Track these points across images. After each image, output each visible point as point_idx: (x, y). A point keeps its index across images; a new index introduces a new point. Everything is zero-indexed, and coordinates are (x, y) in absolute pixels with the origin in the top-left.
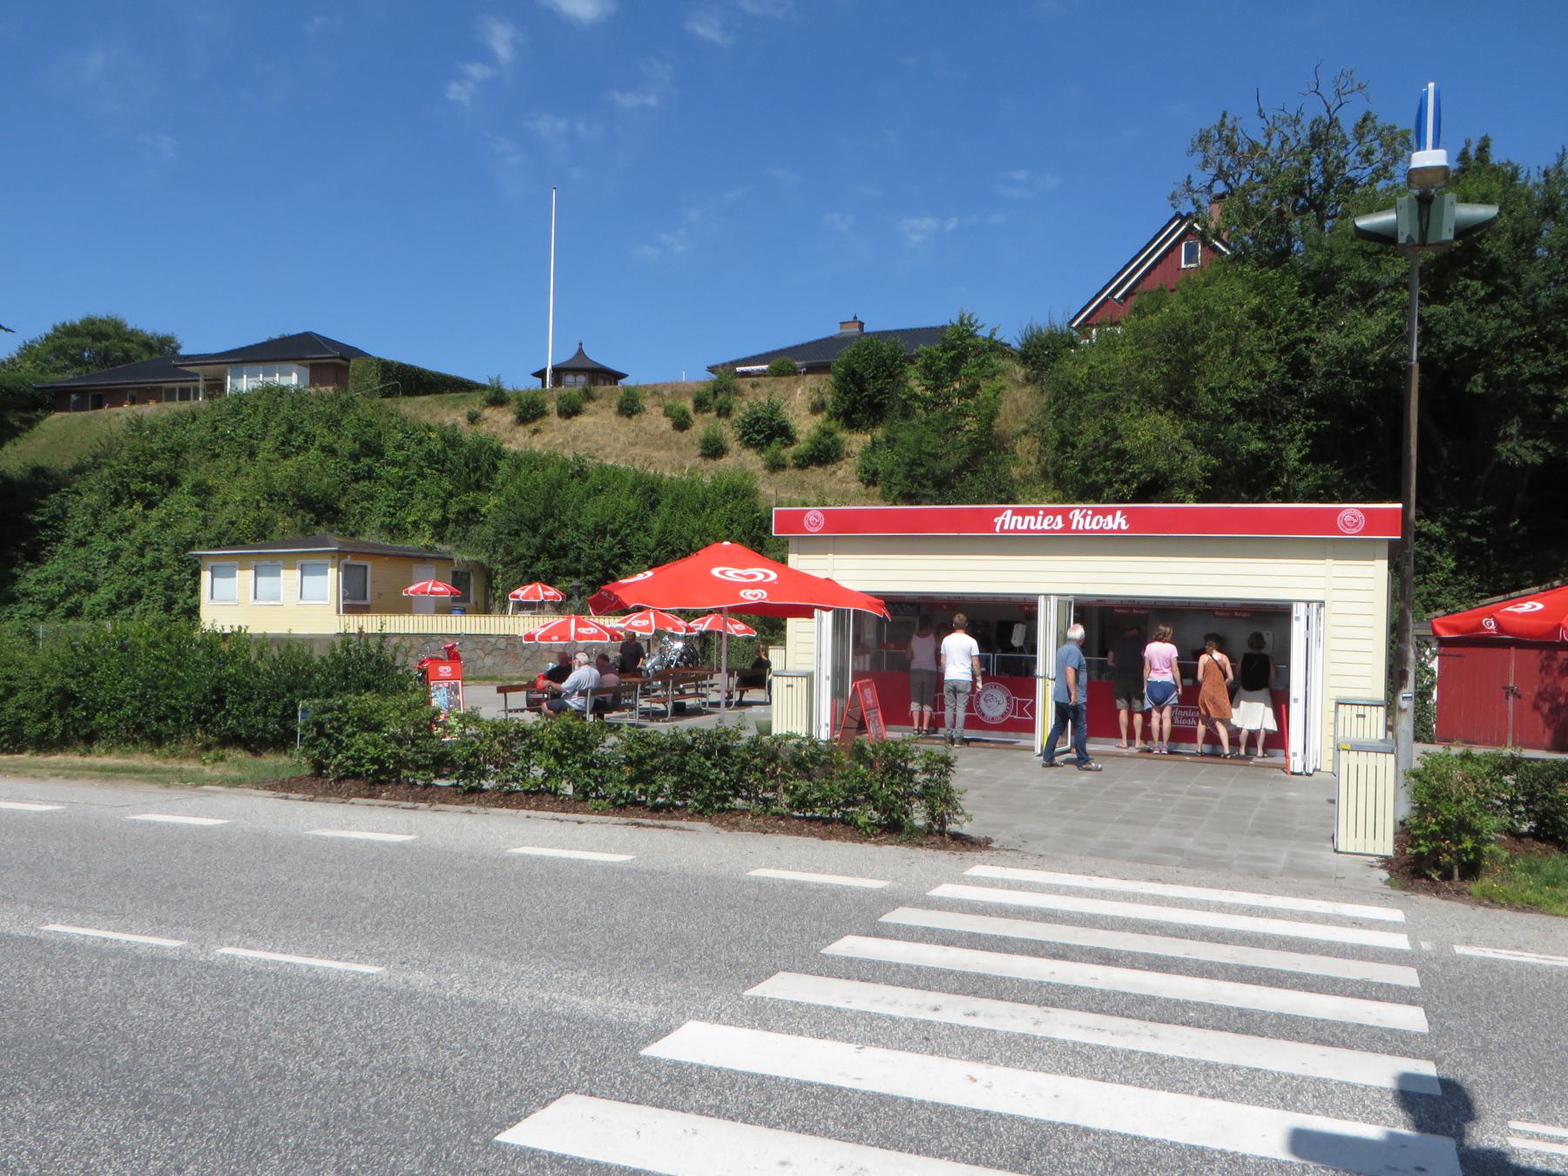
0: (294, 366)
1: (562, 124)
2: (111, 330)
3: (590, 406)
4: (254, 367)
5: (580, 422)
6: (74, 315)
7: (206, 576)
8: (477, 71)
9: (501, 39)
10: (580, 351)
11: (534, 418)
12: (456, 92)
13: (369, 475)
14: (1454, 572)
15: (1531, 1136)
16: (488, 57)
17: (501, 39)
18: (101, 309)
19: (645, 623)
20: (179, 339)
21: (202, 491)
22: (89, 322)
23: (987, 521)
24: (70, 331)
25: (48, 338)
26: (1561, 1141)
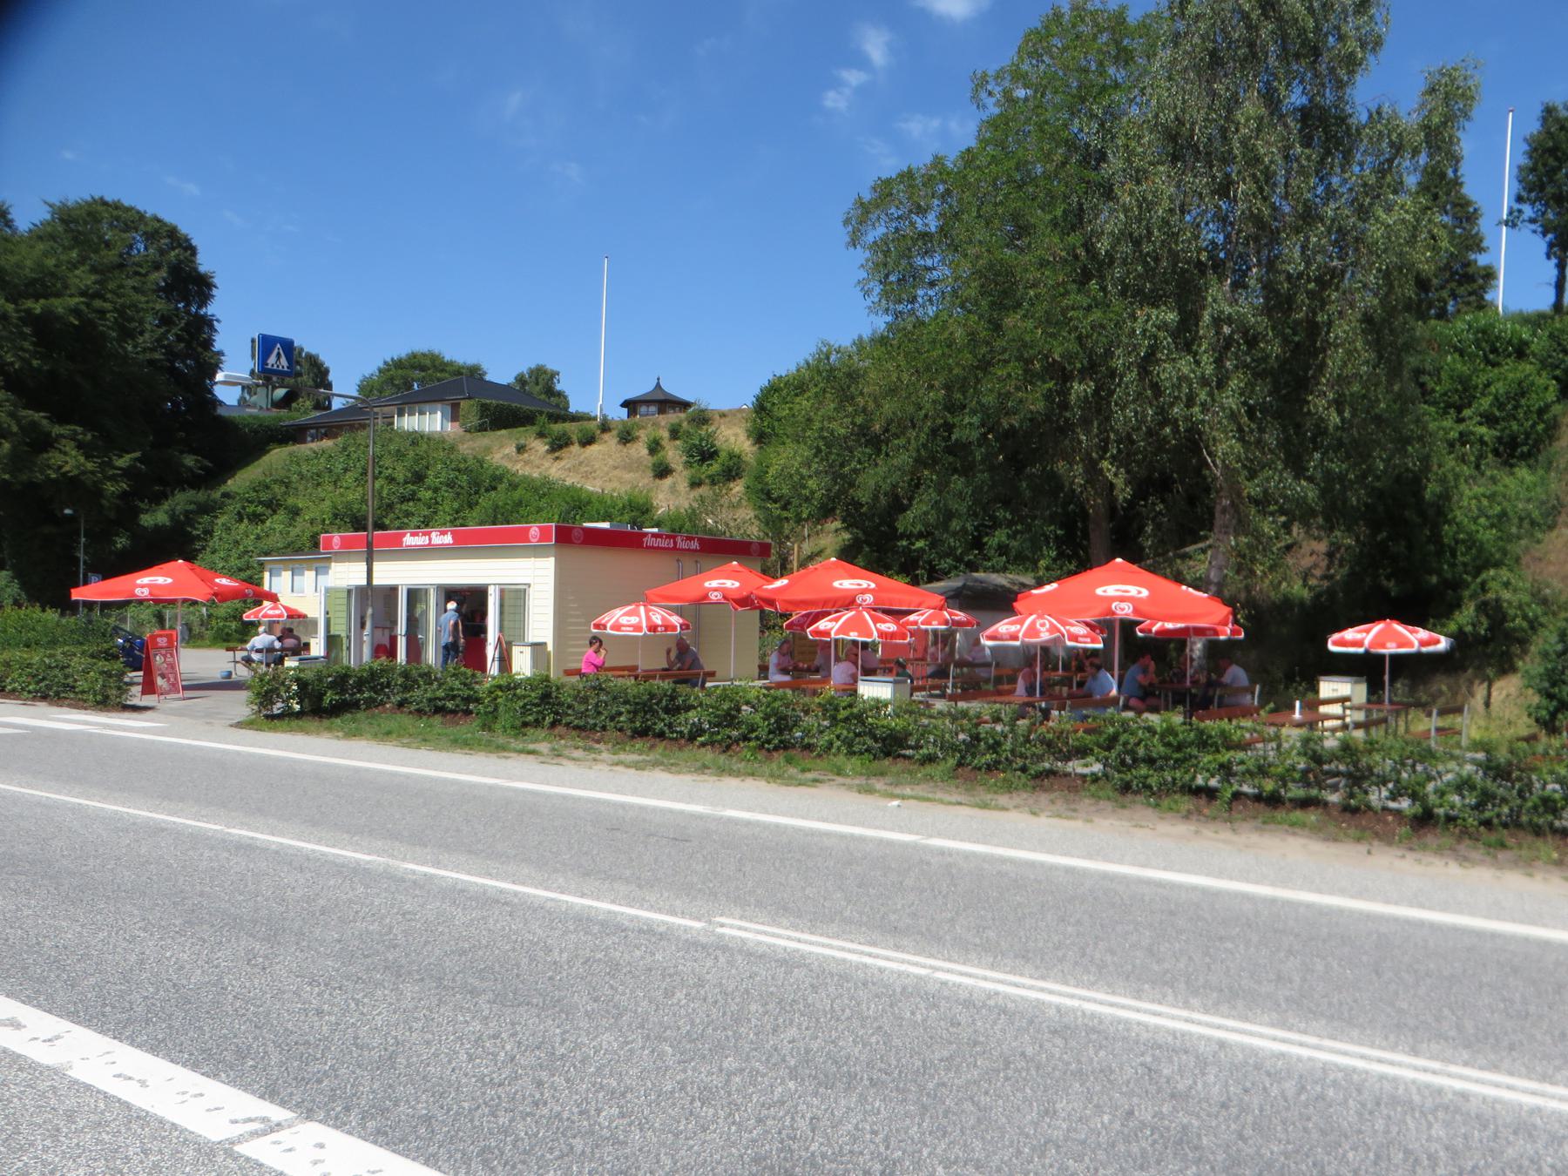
0: (439, 405)
1: (935, 123)
2: (428, 362)
3: (606, 436)
4: (433, 405)
5: (594, 448)
6: (400, 350)
7: (267, 575)
8: (854, 77)
9: (876, 45)
10: (658, 385)
11: (560, 447)
12: (833, 100)
13: (413, 497)
14: (1054, 560)
15: (1400, 1065)
16: (862, 62)
17: (876, 45)
19: (634, 620)
20: (485, 366)
21: (295, 512)
22: (414, 356)
23: (398, 540)
24: (399, 364)
25: (380, 371)
26: (1562, 1099)
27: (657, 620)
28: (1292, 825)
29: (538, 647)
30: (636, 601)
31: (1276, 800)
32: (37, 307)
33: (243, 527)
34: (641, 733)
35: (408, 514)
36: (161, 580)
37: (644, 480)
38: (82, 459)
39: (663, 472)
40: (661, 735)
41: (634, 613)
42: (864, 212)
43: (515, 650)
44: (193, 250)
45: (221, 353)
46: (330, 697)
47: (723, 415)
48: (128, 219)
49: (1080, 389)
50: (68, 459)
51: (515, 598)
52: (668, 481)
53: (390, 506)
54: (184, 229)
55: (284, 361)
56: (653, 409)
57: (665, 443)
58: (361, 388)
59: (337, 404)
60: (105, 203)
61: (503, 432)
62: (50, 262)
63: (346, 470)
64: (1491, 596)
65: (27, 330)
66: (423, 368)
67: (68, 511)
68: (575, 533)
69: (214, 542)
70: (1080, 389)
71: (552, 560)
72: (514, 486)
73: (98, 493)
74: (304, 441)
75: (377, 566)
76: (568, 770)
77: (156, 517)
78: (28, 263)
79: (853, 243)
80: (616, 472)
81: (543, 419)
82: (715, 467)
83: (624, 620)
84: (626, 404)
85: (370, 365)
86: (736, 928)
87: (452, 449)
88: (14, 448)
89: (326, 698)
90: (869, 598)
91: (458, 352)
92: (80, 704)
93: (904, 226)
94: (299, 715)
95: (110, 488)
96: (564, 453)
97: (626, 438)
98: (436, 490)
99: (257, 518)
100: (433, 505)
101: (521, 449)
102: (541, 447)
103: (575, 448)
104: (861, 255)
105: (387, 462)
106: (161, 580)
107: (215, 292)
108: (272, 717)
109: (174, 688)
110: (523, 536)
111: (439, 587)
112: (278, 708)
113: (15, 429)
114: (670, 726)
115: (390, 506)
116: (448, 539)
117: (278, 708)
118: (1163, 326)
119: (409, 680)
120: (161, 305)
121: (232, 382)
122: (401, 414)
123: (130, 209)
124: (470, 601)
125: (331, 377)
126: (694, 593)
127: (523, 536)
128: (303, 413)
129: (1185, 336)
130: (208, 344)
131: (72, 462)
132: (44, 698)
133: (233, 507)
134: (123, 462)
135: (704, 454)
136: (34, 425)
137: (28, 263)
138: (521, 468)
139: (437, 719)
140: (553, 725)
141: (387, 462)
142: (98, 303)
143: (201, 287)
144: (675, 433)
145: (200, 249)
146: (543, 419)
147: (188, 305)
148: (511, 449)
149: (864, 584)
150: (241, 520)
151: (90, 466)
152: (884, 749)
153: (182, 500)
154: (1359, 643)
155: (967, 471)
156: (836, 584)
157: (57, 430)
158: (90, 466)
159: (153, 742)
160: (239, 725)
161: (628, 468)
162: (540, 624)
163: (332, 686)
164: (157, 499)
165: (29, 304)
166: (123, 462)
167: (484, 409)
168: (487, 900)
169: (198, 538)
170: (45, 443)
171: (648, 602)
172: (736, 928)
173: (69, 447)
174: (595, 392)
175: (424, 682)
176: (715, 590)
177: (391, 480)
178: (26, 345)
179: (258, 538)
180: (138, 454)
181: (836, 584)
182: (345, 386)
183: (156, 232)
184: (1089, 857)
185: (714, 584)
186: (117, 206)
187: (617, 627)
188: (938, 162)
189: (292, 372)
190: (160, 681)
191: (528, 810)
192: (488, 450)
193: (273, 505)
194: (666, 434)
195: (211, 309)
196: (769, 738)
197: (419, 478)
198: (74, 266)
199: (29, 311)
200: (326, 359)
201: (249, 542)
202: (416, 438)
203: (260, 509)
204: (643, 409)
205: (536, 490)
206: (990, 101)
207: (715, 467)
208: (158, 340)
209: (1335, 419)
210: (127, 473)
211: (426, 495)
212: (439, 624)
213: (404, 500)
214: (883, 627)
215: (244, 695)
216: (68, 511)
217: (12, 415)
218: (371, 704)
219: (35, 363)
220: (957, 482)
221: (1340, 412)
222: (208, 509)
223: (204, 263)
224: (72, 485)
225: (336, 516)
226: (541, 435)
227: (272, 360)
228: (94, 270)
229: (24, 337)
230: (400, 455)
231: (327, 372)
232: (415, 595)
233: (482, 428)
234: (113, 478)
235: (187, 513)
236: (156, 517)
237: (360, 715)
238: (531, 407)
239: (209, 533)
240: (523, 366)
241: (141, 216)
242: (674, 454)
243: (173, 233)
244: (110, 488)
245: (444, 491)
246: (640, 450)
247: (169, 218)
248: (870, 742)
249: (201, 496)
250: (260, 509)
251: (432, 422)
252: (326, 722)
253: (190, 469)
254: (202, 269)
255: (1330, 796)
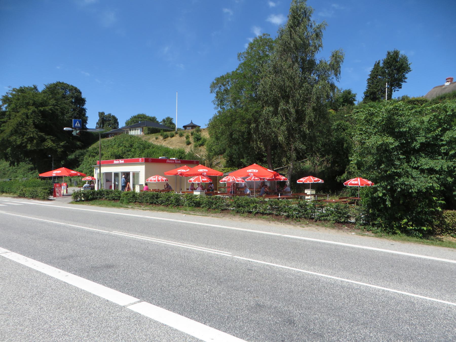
3: (177, 135)
4: (138, 128)
5: (174, 138)
6: (136, 114)
7: (95, 170)
11: (166, 138)
13: (130, 151)
18: (141, 112)
19: (155, 179)
20: (156, 117)
22: (139, 115)
23: (113, 162)
24: (135, 117)
27: (160, 179)
28: (263, 218)
29: (141, 186)
30: (156, 175)
31: (290, 217)
32: (42, 109)
33: (90, 159)
34: (152, 203)
35: (129, 155)
36: (58, 172)
37: (184, 145)
38: (52, 144)
39: (189, 143)
40: (155, 204)
41: (155, 177)
42: (213, 86)
43: (136, 186)
44: (81, 93)
45: (87, 117)
46: (90, 197)
47: (204, 129)
48: (64, 87)
49: (253, 125)
50: (49, 144)
51: (136, 175)
52: (190, 146)
53: (125, 153)
54: (79, 88)
55: (79, 125)
56: (190, 128)
57: (190, 137)
58: (126, 123)
59: (120, 127)
60: (60, 83)
61: (153, 134)
62: (45, 98)
63: (115, 144)
64: (350, 170)
65: (40, 114)
66: (141, 118)
67: (50, 156)
68: (149, 160)
69: (84, 162)
70: (253, 125)
71: (144, 166)
72: (153, 148)
73: (56, 151)
74: (108, 137)
75: (102, 168)
76: (135, 211)
77: (71, 157)
78: (40, 99)
79: (211, 92)
80: (178, 144)
81: (162, 131)
82: (200, 142)
83: (152, 179)
84: (184, 127)
85: (128, 117)
86: (115, 233)
87: (140, 139)
88: (37, 141)
89: (91, 197)
90: (205, 173)
91: (150, 114)
92: (39, 199)
93: (224, 88)
94: (83, 201)
95: (59, 150)
96: (166, 139)
97: (181, 135)
98: (135, 149)
99: (94, 156)
100: (135, 152)
101: (157, 138)
102: (161, 138)
103: (169, 138)
104: (214, 95)
105: (124, 142)
106: (58, 172)
107: (86, 102)
108: (77, 201)
109: (60, 195)
110: (138, 161)
111: (122, 172)
112: (78, 199)
113: (37, 137)
114: (157, 201)
115: (125, 153)
116: (123, 162)
117: (78, 199)
118: (270, 111)
119: (108, 193)
120: (73, 106)
121: (92, 124)
122: (130, 130)
123: (65, 84)
124: (127, 175)
125: (118, 121)
126: (175, 173)
127: (138, 161)
128: (108, 129)
129: (275, 113)
130: (85, 114)
131: (50, 144)
132: (33, 198)
133: (88, 154)
134: (62, 144)
135: (198, 139)
136: (41, 136)
137: (40, 99)
138: (156, 143)
139: (113, 201)
140: (135, 202)
141: (124, 142)
142: (56, 107)
143: (82, 101)
144: (192, 134)
145: (82, 92)
146: (162, 131)
147: (80, 106)
148: (154, 139)
149: (205, 170)
150: (90, 157)
151: (54, 145)
152: (196, 205)
153: (78, 152)
154: (302, 181)
155: (238, 143)
156: (199, 170)
157: (47, 137)
158: (54, 145)
159: (186, 223)
160: (70, 203)
161: (181, 142)
162: (142, 181)
163: (91, 194)
164: (73, 152)
165: (40, 108)
166: (62, 144)
167: (149, 129)
168: (43, 223)
169: (80, 161)
170: (44, 140)
171: (159, 175)
172: (115, 233)
173: (49, 141)
174: (179, 124)
175: (117, 195)
176: (251, 173)
177: (125, 146)
178: (40, 118)
179: (93, 161)
180: (65, 142)
181: (199, 170)
182: (122, 124)
183: (72, 89)
184: (182, 220)
185: (250, 171)
186: (63, 83)
187: (151, 180)
188: (228, 73)
189: (107, 120)
190: (57, 194)
191: (87, 214)
192: (149, 139)
193: (97, 153)
194: (190, 134)
195: (85, 107)
196: (176, 204)
197: (131, 146)
198: (50, 99)
199: (40, 110)
200: (117, 116)
201: (92, 162)
202: (132, 136)
203: (94, 154)
204: (188, 128)
205: (158, 148)
206: (242, 59)
207: (200, 142)
208: (72, 115)
209: (308, 132)
210: (63, 146)
211: (133, 150)
212: (121, 179)
213: (128, 151)
214: (203, 179)
215: (71, 197)
216: (50, 156)
217: (36, 134)
218: (100, 198)
219: (42, 122)
220: (234, 147)
221: (309, 130)
222: (83, 154)
223: (83, 96)
224: (51, 150)
225: (111, 155)
226: (161, 135)
227: (76, 124)
228: (55, 100)
229: (39, 116)
230: (127, 140)
231: (117, 119)
232: (116, 175)
233: (148, 134)
234: (60, 148)
235: (79, 155)
236: (71, 157)
237: (97, 201)
238: (166, 128)
239: (83, 160)
240: (165, 117)
241: (68, 85)
242: (191, 139)
243: (76, 89)
244: (59, 150)
245: (137, 149)
246: (184, 138)
247: (75, 85)
248: (193, 204)
249: (82, 151)
250: (94, 154)
251: (137, 132)
252: (88, 202)
253: (78, 145)
254: (83, 97)
255: (305, 216)
